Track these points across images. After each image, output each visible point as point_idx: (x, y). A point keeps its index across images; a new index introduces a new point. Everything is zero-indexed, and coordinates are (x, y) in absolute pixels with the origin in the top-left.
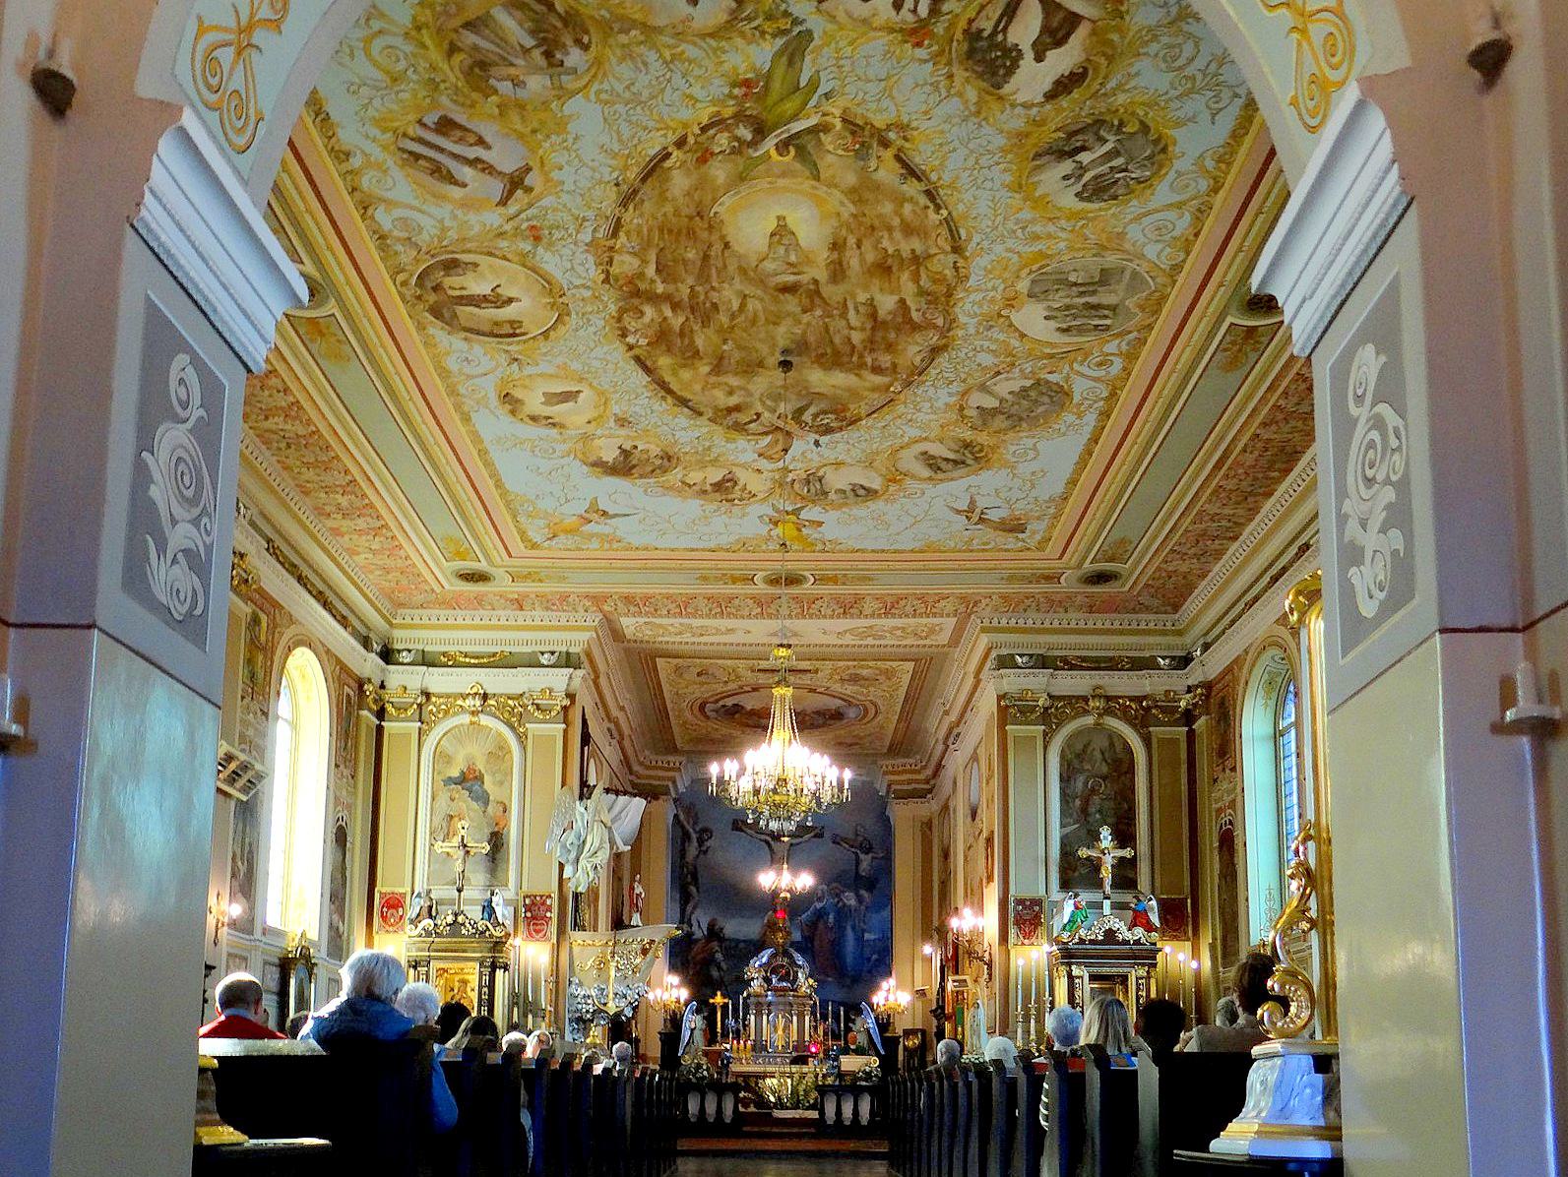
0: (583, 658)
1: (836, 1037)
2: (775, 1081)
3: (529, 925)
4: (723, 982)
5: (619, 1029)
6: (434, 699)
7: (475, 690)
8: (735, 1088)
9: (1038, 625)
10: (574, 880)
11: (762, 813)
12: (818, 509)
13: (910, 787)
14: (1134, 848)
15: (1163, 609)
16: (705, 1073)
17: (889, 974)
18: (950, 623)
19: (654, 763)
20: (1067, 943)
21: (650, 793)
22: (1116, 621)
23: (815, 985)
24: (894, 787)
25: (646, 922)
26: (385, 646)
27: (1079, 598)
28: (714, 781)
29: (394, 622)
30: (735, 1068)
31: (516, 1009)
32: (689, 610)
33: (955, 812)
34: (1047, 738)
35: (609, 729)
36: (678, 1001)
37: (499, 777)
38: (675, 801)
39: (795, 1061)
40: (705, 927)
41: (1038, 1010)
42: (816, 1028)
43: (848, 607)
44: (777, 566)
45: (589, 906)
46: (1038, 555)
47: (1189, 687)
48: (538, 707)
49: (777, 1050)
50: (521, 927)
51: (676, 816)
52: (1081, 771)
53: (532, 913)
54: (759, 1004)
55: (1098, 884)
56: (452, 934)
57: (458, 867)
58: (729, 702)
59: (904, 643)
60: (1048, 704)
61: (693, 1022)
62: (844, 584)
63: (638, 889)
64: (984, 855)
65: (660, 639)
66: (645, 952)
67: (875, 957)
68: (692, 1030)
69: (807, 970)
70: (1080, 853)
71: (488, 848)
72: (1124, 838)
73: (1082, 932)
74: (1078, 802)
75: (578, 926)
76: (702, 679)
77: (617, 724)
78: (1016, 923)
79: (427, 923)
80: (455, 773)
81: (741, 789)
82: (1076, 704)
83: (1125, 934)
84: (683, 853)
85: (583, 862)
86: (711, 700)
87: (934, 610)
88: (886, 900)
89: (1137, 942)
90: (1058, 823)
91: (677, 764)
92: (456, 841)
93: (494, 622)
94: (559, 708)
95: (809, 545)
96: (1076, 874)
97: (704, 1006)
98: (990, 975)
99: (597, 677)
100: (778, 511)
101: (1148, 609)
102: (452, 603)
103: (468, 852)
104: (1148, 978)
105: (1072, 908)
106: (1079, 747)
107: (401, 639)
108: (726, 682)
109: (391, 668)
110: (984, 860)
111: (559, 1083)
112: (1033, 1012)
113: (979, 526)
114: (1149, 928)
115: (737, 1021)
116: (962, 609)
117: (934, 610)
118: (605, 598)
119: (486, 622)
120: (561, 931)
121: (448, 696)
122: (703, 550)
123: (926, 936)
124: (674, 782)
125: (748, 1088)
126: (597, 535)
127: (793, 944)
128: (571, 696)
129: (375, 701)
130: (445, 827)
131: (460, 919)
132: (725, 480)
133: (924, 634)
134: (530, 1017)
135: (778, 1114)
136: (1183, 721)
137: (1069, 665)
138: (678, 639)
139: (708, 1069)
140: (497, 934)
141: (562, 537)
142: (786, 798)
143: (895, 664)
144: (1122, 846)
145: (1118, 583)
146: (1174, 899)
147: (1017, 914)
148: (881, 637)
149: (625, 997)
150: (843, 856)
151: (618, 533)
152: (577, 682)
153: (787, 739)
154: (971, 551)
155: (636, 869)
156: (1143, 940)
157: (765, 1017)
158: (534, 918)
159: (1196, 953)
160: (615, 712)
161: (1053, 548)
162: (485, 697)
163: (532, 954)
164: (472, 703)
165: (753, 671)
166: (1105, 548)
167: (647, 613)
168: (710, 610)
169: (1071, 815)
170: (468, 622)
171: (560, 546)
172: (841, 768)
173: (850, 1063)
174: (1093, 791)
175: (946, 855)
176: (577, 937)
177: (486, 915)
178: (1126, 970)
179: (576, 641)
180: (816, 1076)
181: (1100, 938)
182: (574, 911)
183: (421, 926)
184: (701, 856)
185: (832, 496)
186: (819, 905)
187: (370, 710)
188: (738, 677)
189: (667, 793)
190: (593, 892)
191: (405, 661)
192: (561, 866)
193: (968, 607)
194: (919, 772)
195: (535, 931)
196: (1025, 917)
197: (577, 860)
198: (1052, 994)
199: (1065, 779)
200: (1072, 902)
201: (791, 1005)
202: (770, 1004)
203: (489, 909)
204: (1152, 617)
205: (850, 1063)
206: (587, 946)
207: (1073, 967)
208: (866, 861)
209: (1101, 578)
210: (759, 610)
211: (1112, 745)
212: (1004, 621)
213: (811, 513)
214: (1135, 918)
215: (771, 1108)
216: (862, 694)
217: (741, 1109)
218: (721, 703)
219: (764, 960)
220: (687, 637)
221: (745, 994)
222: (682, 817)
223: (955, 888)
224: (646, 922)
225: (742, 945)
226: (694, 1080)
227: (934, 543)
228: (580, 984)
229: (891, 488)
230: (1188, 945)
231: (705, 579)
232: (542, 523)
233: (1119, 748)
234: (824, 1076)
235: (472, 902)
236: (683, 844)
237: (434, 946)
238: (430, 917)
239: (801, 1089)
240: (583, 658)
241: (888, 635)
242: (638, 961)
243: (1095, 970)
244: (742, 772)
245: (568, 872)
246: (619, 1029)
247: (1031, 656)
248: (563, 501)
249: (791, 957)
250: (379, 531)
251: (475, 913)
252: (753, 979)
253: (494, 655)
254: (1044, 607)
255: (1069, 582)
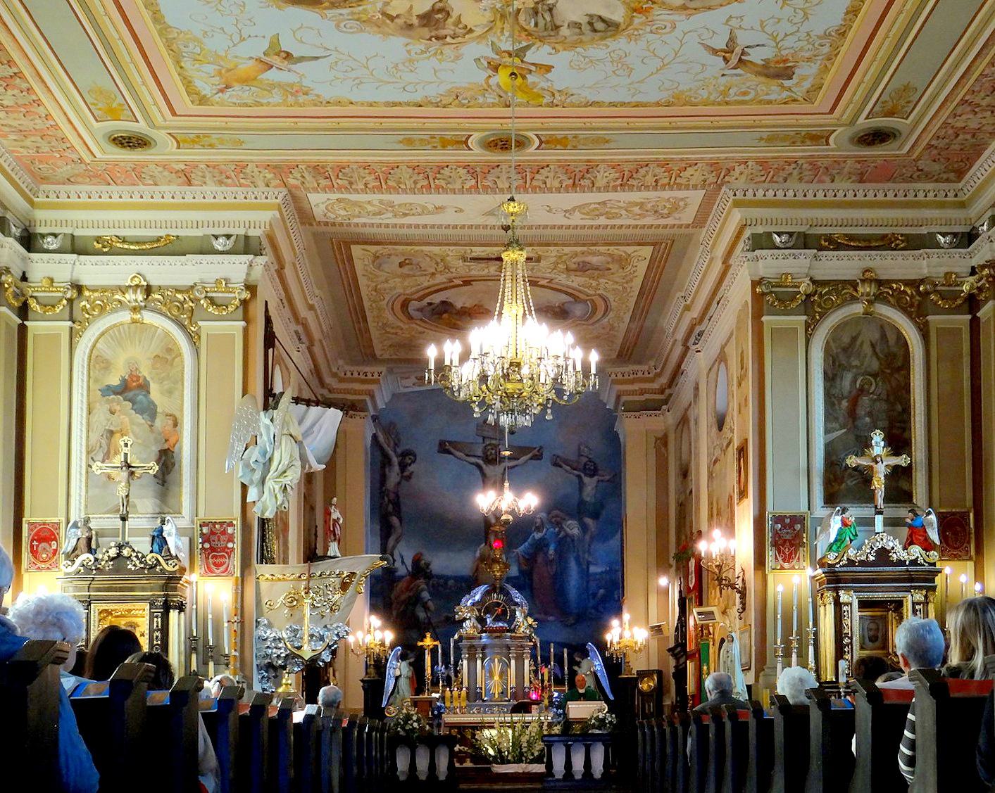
0: (265, 243)
1: (559, 681)
2: (494, 732)
3: (207, 558)
4: (430, 623)
5: (314, 676)
6: (87, 293)
7: (136, 282)
8: (449, 741)
9: (800, 197)
10: (259, 505)
11: (490, 406)
12: (547, 48)
13: (643, 398)
14: (910, 455)
15: (945, 176)
16: (415, 725)
17: (618, 612)
18: (696, 197)
19: (349, 374)
20: (833, 565)
21: (349, 408)
22: (889, 190)
23: (535, 624)
24: (624, 398)
25: (344, 553)
26: (26, 230)
27: (849, 162)
28: (432, 366)
29: (36, 200)
30: (448, 718)
31: (194, 657)
32: (390, 183)
33: (696, 423)
34: (810, 329)
35: (297, 333)
36: (383, 644)
37: (167, 385)
38: (375, 418)
39: (516, 709)
40: (409, 562)
41: (800, 642)
42: (536, 672)
43: (578, 178)
44: (495, 124)
45: (278, 538)
46: (807, 107)
47: (973, 268)
48: (212, 301)
49: (496, 695)
50: (198, 560)
51: (375, 437)
52: (847, 368)
53: (211, 544)
54: (472, 648)
55: (869, 497)
56: (116, 570)
57: (121, 491)
58: (437, 299)
59: (640, 223)
60: (810, 290)
61: (398, 669)
62: (575, 148)
63: (336, 515)
64: (735, 468)
65: (356, 220)
66: (344, 586)
67: (602, 591)
68: (397, 678)
69: (526, 609)
70: (848, 462)
71: (157, 468)
72: (898, 443)
73: (851, 553)
74: (845, 404)
75: (265, 558)
76: (406, 270)
77: (305, 326)
78: (775, 544)
79: (85, 557)
80: (114, 380)
81: (465, 376)
82: (843, 289)
83: (899, 553)
84: (383, 479)
85: (270, 483)
86: (415, 296)
87: (679, 180)
88: (616, 525)
89: (914, 562)
90: (822, 429)
91: (376, 376)
92: (118, 460)
93: (157, 200)
94: (237, 302)
95: (534, 96)
96: (844, 485)
97: (409, 650)
98: (744, 604)
99: (282, 267)
100: (498, 52)
101: (928, 177)
102: (107, 176)
103: (132, 473)
104: (926, 603)
105: (839, 525)
106: (846, 340)
107: (44, 221)
108: (433, 274)
109: (34, 256)
110: (736, 474)
111: (251, 733)
112: (795, 644)
113: (738, 71)
114: (928, 546)
115: (447, 668)
116: (712, 179)
117: (679, 180)
118: (291, 167)
119: (147, 199)
120: (246, 565)
121: (104, 289)
122: (408, 104)
123: (662, 565)
124: (373, 397)
125: (463, 741)
126: (280, 86)
127: (509, 580)
128: (251, 288)
129: (16, 296)
130: (105, 444)
131: (126, 552)
132: (434, 10)
133: (666, 211)
134: (211, 664)
135: (499, 769)
136: (966, 306)
137: (834, 244)
138: (376, 220)
139: (418, 721)
140: (170, 569)
141: (237, 87)
142: (519, 386)
143: (630, 249)
144: (896, 453)
145: (896, 144)
146: (954, 514)
147: (776, 534)
148: (619, 216)
149: (322, 638)
150: (564, 480)
151: (306, 83)
152: (258, 271)
153: (521, 312)
154: (727, 103)
155: (330, 492)
156: (920, 560)
157: (479, 662)
158: (213, 549)
159: (979, 575)
160: (303, 312)
161: (823, 100)
162: (148, 290)
163: (211, 592)
164: (133, 297)
165: (465, 260)
166: (885, 97)
167: (340, 188)
168: (415, 183)
169: (836, 419)
170: (126, 199)
171: (235, 100)
172: (587, 349)
173: (579, 710)
174: (862, 391)
175: (685, 473)
176: (265, 570)
177: (156, 547)
178: (901, 594)
179: (257, 219)
180: (541, 727)
181: (872, 558)
182: (262, 541)
183: (78, 561)
184: (404, 482)
185: (564, 31)
186: (538, 536)
187: (10, 306)
188: (447, 268)
189: (364, 410)
190: (282, 516)
191: (51, 248)
192: (244, 488)
193: (720, 173)
194: (652, 380)
195: (215, 564)
196: (782, 537)
197: (263, 481)
198: (816, 624)
199: (830, 379)
200: (838, 518)
201: (508, 648)
202: (484, 647)
203: (159, 539)
204: (930, 186)
205: (579, 710)
206: (277, 582)
207: (841, 593)
208: (590, 483)
209: (877, 137)
210: (474, 182)
211: (884, 336)
212: (760, 193)
213: (539, 54)
214: (911, 535)
215: (490, 763)
216: (590, 287)
217: (457, 765)
218: (427, 300)
219: (477, 598)
220: (388, 219)
221: (456, 637)
222: (381, 438)
223: (698, 509)
224: (344, 553)
225: (451, 582)
226: (402, 733)
227: (682, 92)
228: (270, 626)
229: (636, 21)
230: (970, 565)
231: (409, 142)
232: (211, 68)
233: (892, 339)
234: (550, 725)
235: (137, 532)
236: (383, 467)
237: (95, 584)
238: (90, 550)
239: (524, 739)
240: (265, 243)
241: (623, 212)
242: (337, 597)
243: (866, 595)
244: (465, 357)
245: (252, 495)
246: (314, 676)
247: (791, 234)
248: (236, 38)
249: (507, 594)
250: (11, 82)
251: (142, 545)
252: (465, 620)
253: (158, 239)
254: (808, 174)
255: (839, 144)
